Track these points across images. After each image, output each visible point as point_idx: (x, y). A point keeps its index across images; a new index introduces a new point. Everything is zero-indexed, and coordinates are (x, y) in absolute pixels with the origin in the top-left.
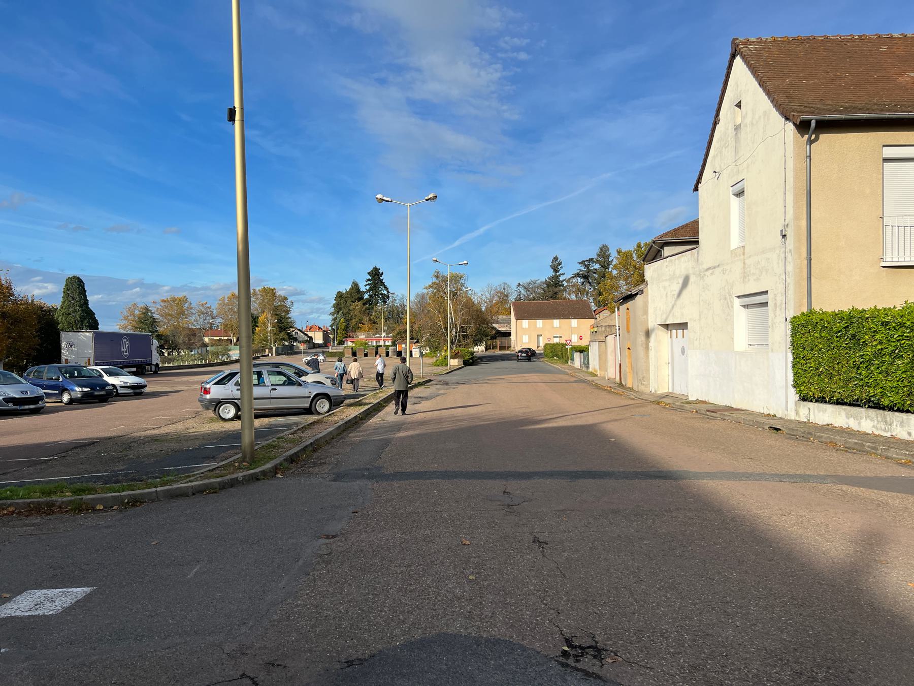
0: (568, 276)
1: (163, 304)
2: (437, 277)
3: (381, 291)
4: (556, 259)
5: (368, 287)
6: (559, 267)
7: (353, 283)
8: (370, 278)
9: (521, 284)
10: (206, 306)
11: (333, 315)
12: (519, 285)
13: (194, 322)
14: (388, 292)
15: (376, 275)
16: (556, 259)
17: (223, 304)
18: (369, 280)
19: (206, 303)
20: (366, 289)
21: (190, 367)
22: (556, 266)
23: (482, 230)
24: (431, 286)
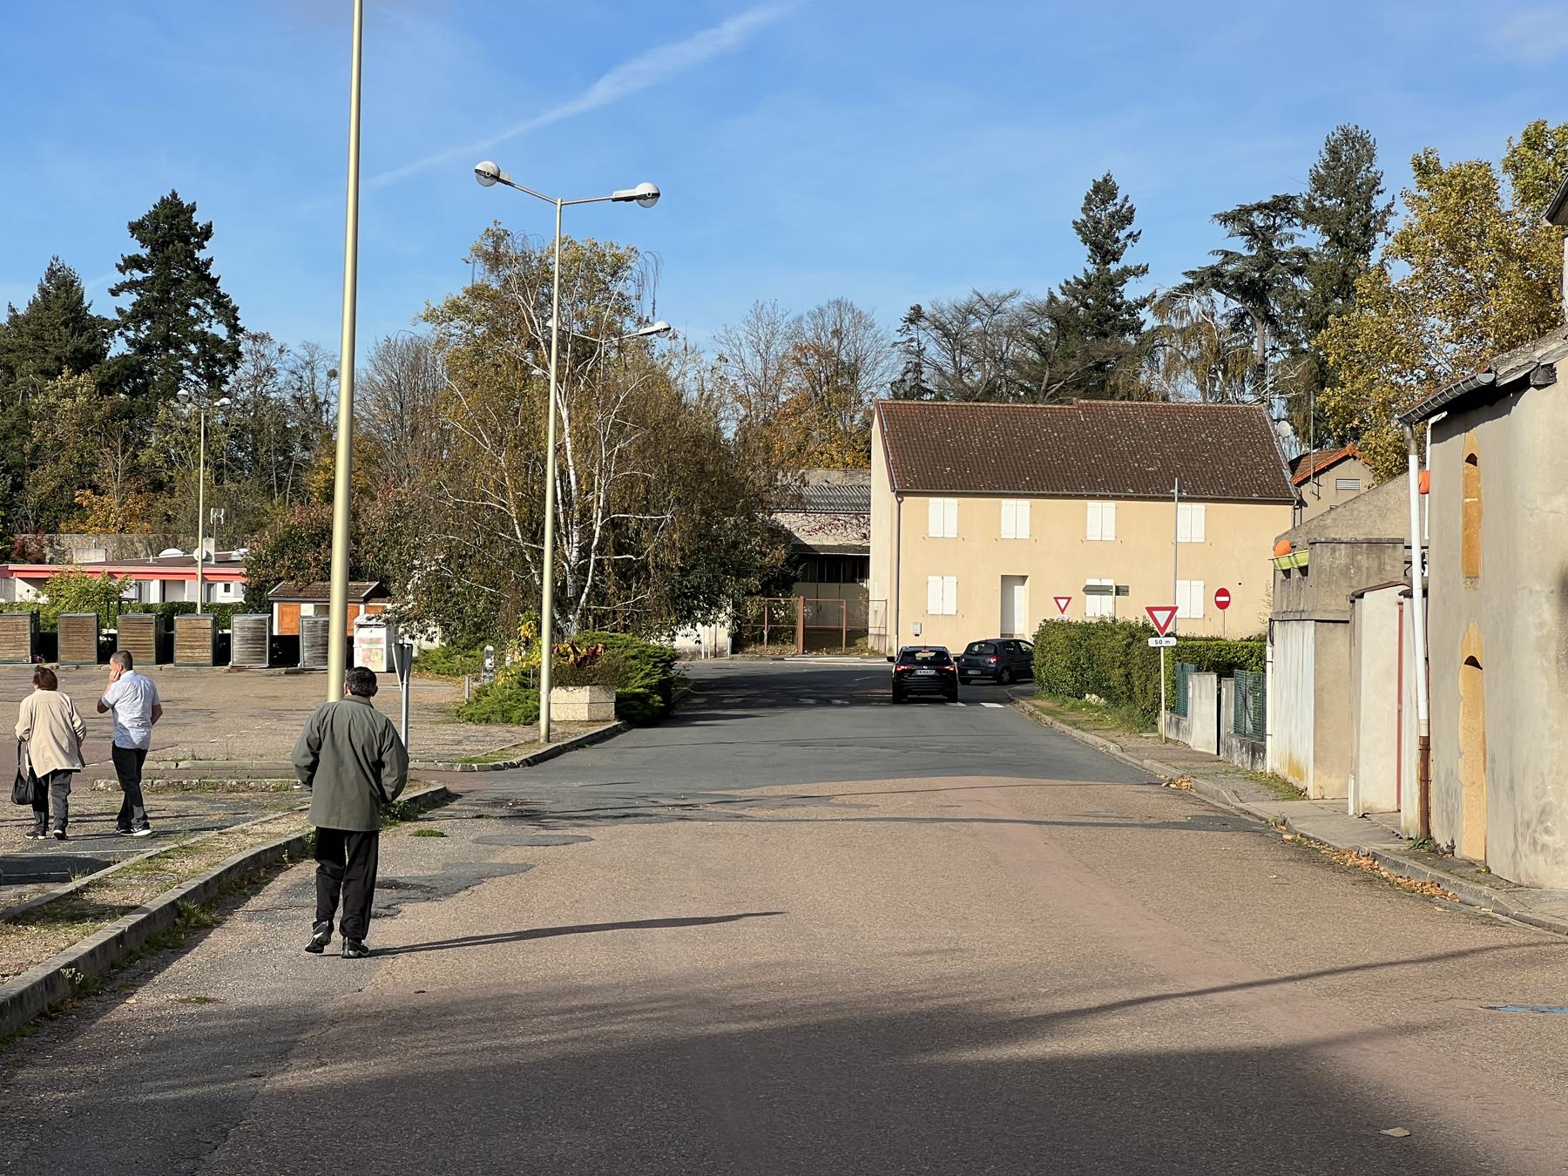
0: (1164, 278)
2: (495, 260)
3: (195, 321)
4: (1104, 190)
5: (128, 300)
7: (52, 273)
8: (144, 252)
9: (927, 309)
12: (916, 315)
14: (235, 329)
16: (1104, 190)
18: (134, 262)
24: (456, 309)
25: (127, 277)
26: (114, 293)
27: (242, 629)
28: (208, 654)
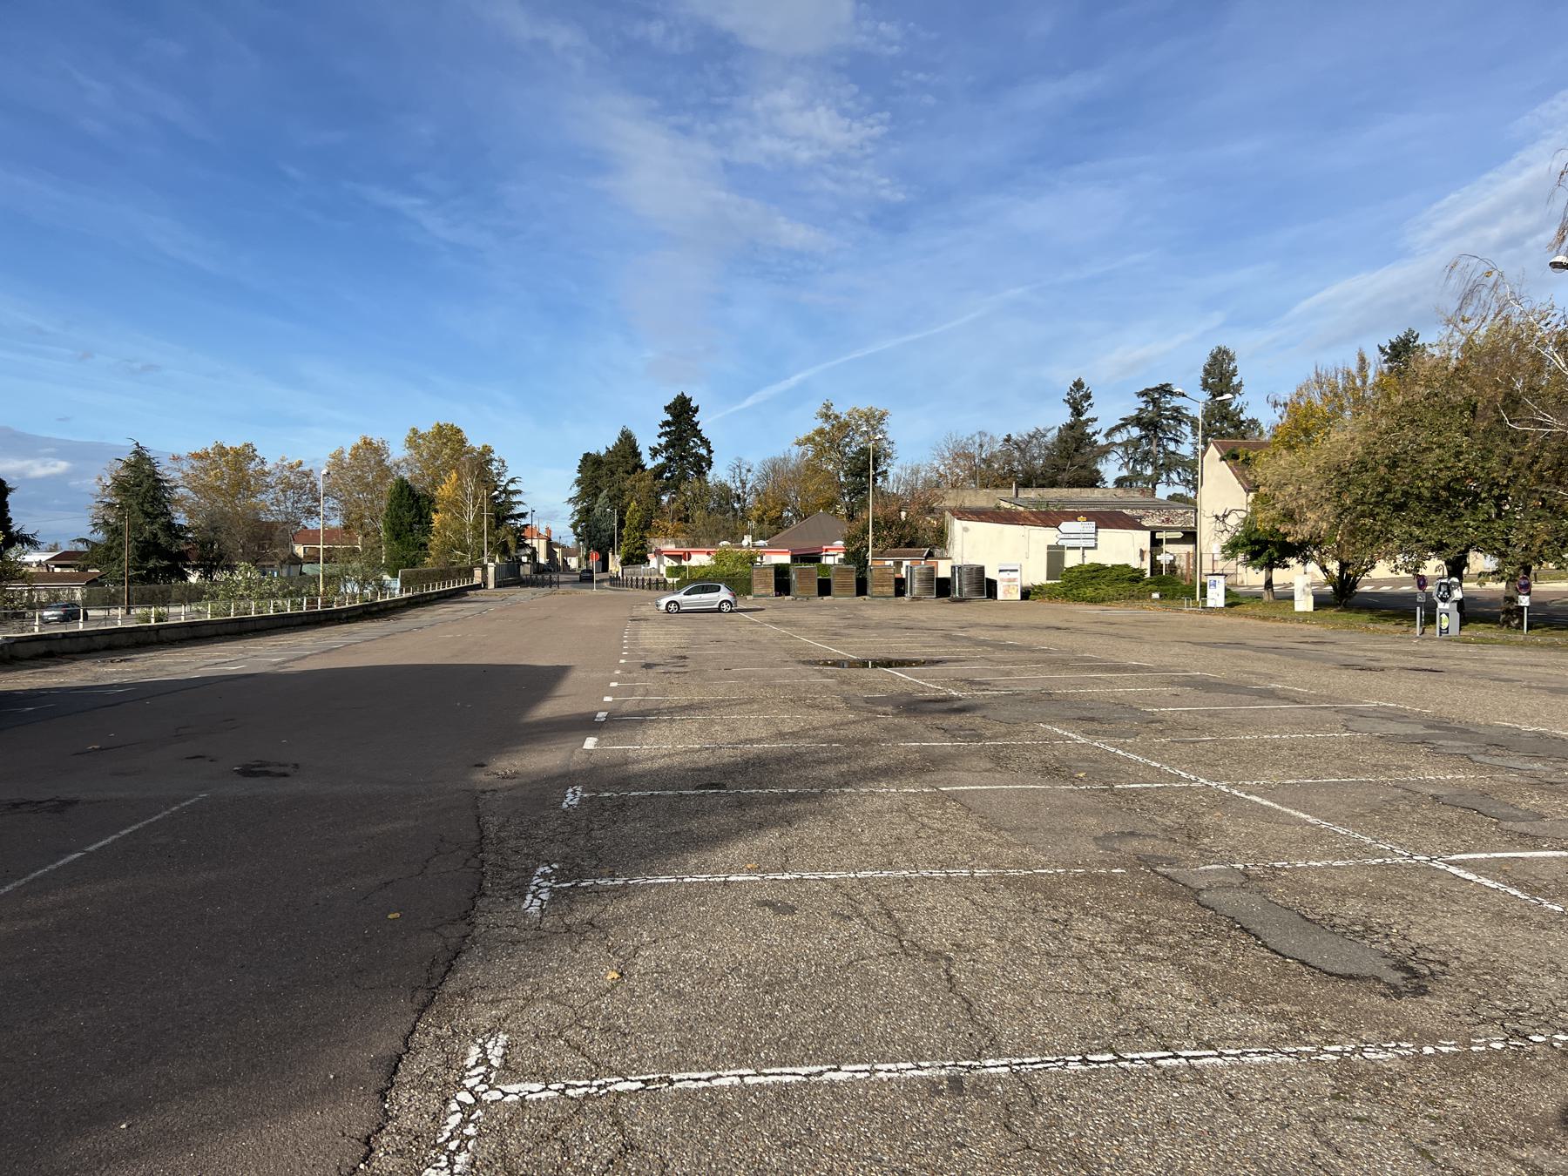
0: (1103, 425)
1: (196, 464)
2: (827, 417)
3: (693, 448)
4: (1078, 385)
5: (663, 440)
6: (1085, 405)
7: (623, 433)
8: (670, 419)
9: (1014, 437)
10: (300, 469)
11: (577, 504)
12: (1008, 439)
13: (271, 505)
14: (710, 452)
15: (682, 412)
16: (1078, 385)
17: (337, 462)
18: (666, 423)
19: (301, 463)
20: (660, 445)
21: (250, 626)
22: (1079, 399)
23: (794, 380)
24: (809, 440)
25: (663, 431)
26: (659, 437)
27: (920, 574)
28: (892, 590)
